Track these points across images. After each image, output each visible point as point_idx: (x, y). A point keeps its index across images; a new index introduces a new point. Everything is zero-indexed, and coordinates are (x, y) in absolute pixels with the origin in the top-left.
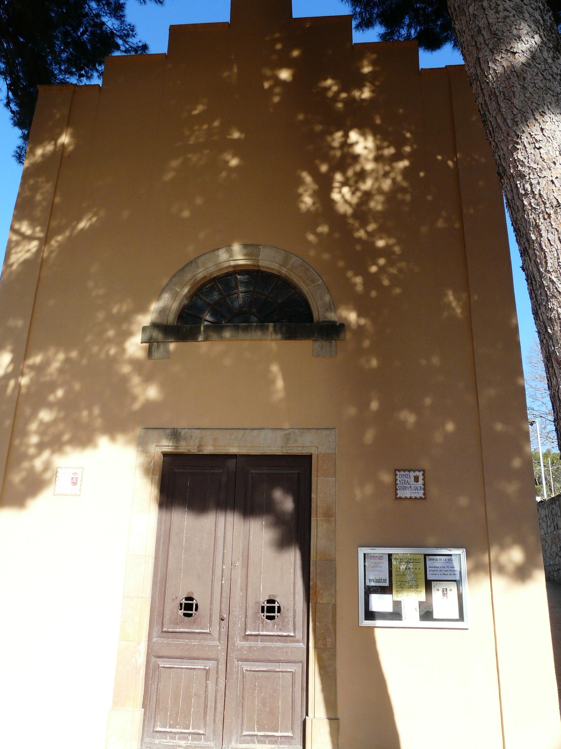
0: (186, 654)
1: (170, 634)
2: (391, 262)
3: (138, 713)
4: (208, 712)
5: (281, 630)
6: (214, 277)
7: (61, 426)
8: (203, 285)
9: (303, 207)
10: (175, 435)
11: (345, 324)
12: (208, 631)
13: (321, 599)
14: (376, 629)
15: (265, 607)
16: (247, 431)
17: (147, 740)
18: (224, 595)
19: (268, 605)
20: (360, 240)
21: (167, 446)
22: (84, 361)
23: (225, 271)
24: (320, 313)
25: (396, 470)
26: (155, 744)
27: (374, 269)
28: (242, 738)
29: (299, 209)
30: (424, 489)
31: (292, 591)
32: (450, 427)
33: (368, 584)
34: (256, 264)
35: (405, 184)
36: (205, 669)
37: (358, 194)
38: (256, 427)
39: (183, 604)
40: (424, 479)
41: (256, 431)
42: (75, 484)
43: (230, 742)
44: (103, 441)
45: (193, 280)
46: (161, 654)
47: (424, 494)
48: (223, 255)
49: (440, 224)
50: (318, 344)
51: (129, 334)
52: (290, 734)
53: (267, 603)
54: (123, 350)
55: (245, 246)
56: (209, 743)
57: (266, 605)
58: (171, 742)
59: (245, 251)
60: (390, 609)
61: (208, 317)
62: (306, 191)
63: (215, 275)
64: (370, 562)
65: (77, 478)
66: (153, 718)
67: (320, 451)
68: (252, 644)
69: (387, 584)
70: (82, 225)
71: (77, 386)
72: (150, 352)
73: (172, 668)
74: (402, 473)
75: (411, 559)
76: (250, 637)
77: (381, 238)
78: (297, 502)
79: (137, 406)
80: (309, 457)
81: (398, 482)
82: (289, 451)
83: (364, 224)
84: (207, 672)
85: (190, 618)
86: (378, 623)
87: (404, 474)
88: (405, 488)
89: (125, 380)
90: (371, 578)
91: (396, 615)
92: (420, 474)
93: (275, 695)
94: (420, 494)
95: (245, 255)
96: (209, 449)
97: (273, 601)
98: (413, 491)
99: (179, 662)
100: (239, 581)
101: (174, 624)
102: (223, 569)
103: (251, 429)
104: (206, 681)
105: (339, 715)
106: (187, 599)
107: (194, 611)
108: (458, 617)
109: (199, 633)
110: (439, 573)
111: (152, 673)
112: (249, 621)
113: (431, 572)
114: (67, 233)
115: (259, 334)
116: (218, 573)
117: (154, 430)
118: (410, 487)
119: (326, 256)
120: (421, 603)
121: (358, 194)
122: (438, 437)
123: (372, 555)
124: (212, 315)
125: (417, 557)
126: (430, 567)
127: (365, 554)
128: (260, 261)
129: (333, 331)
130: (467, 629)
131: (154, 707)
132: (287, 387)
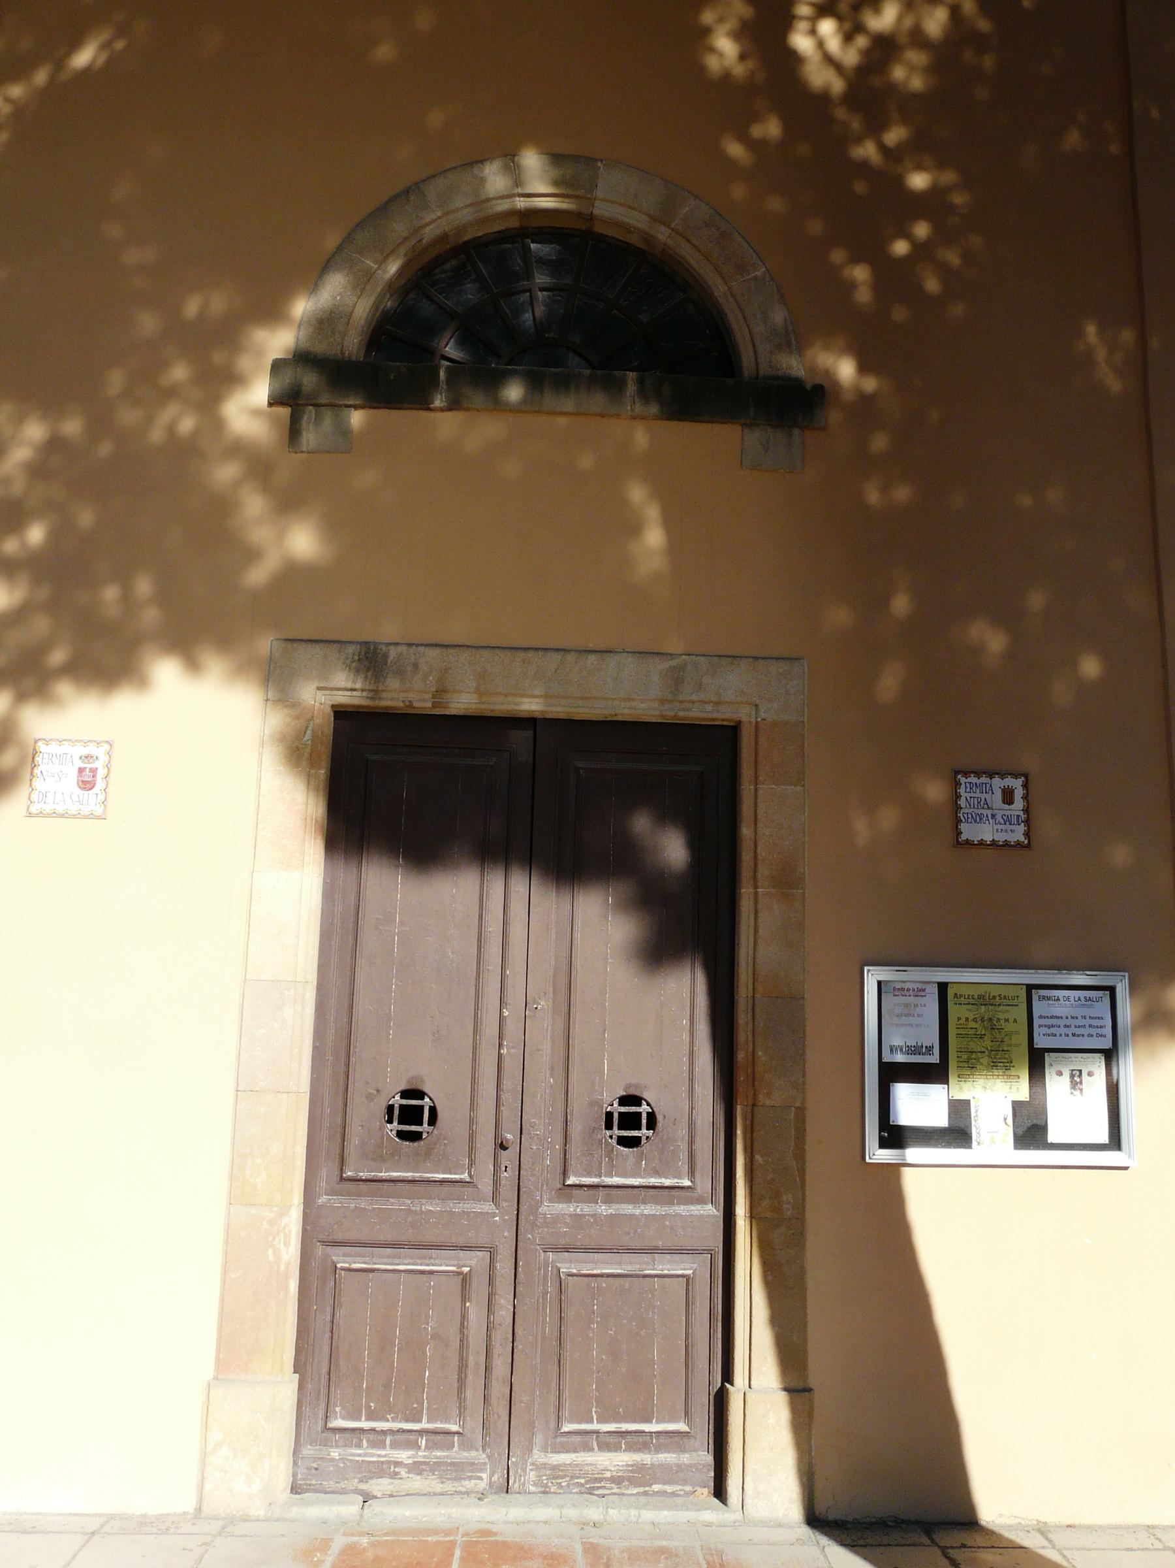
0: (408, 1235)
1: (363, 1187)
2: (944, 234)
3: (287, 1389)
4: (470, 1377)
5: (657, 1173)
6: (466, 243)
7: (41, 625)
8: (437, 261)
9: (713, 64)
10: (371, 660)
11: (826, 386)
12: (465, 1176)
13: (769, 1095)
14: (907, 1173)
15: (616, 1116)
16: (570, 658)
17: (308, 1450)
18: (507, 1083)
19: (623, 1109)
20: (863, 167)
21: (343, 687)
22: (105, 449)
23: (497, 227)
24: (759, 350)
25: (957, 773)
26: (333, 1460)
27: (901, 248)
28: (558, 1440)
29: (703, 69)
30: (1027, 822)
31: (686, 1075)
32: (1091, 667)
33: (887, 1058)
34: (585, 211)
35: (984, 25)
36: (460, 1273)
37: (861, 41)
38: (591, 646)
39: (396, 1106)
40: (1025, 797)
41: (592, 658)
42: (87, 785)
43: (529, 1450)
44: (166, 672)
45: (413, 242)
46: (339, 1237)
47: (1027, 834)
48: (495, 180)
49: (1073, 139)
50: (754, 437)
51: (230, 379)
52: (682, 1426)
53: (620, 1104)
54: (217, 424)
55: (556, 159)
56: (473, 1454)
57: (617, 1109)
58: (373, 1455)
59: (555, 173)
60: (940, 1119)
61: (451, 350)
62: (721, 20)
63: (468, 237)
64: (887, 1006)
65: (94, 771)
66: (323, 1398)
67: (763, 715)
68: (585, 1209)
69: (935, 1058)
70: (83, 58)
71: (86, 518)
72: (294, 432)
73: (373, 1270)
74: (973, 779)
75: (994, 997)
76: (575, 1192)
77: (919, 167)
78: (695, 845)
79: (258, 575)
80: (731, 733)
81: (962, 802)
82: (681, 714)
83: (875, 127)
84: (465, 1280)
85: (416, 1144)
86: (913, 1154)
87: (978, 781)
88: (978, 819)
89: (222, 507)
90: (896, 1044)
91: (957, 1133)
92: (1017, 784)
93: (643, 1333)
94: (1018, 834)
95: (556, 183)
96: (463, 702)
97: (635, 1100)
98: (999, 827)
99: (388, 1257)
100: (547, 1047)
101: (373, 1160)
102: (502, 1019)
103: (580, 651)
104: (464, 1301)
105: (812, 1382)
106: (405, 1094)
107: (425, 1125)
108: (1103, 1137)
109: (442, 1182)
110: (1063, 1030)
111: (318, 1284)
112: (575, 1149)
113: (1044, 1030)
114: (41, 77)
115: (598, 400)
116: (490, 1029)
117: (310, 645)
118: (993, 816)
119: (776, 204)
120: (1017, 1106)
121: (861, 41)
122: (1061, 694)
123: (898, 986)
124: (462, 344)
125: (1011, 992)
126: (1040, 1017)
127: (879, 983)
128: (597, 203)
129: (794, 404)
130: (1126, 1168)
131: (325, 1370)
132: (674, 546)
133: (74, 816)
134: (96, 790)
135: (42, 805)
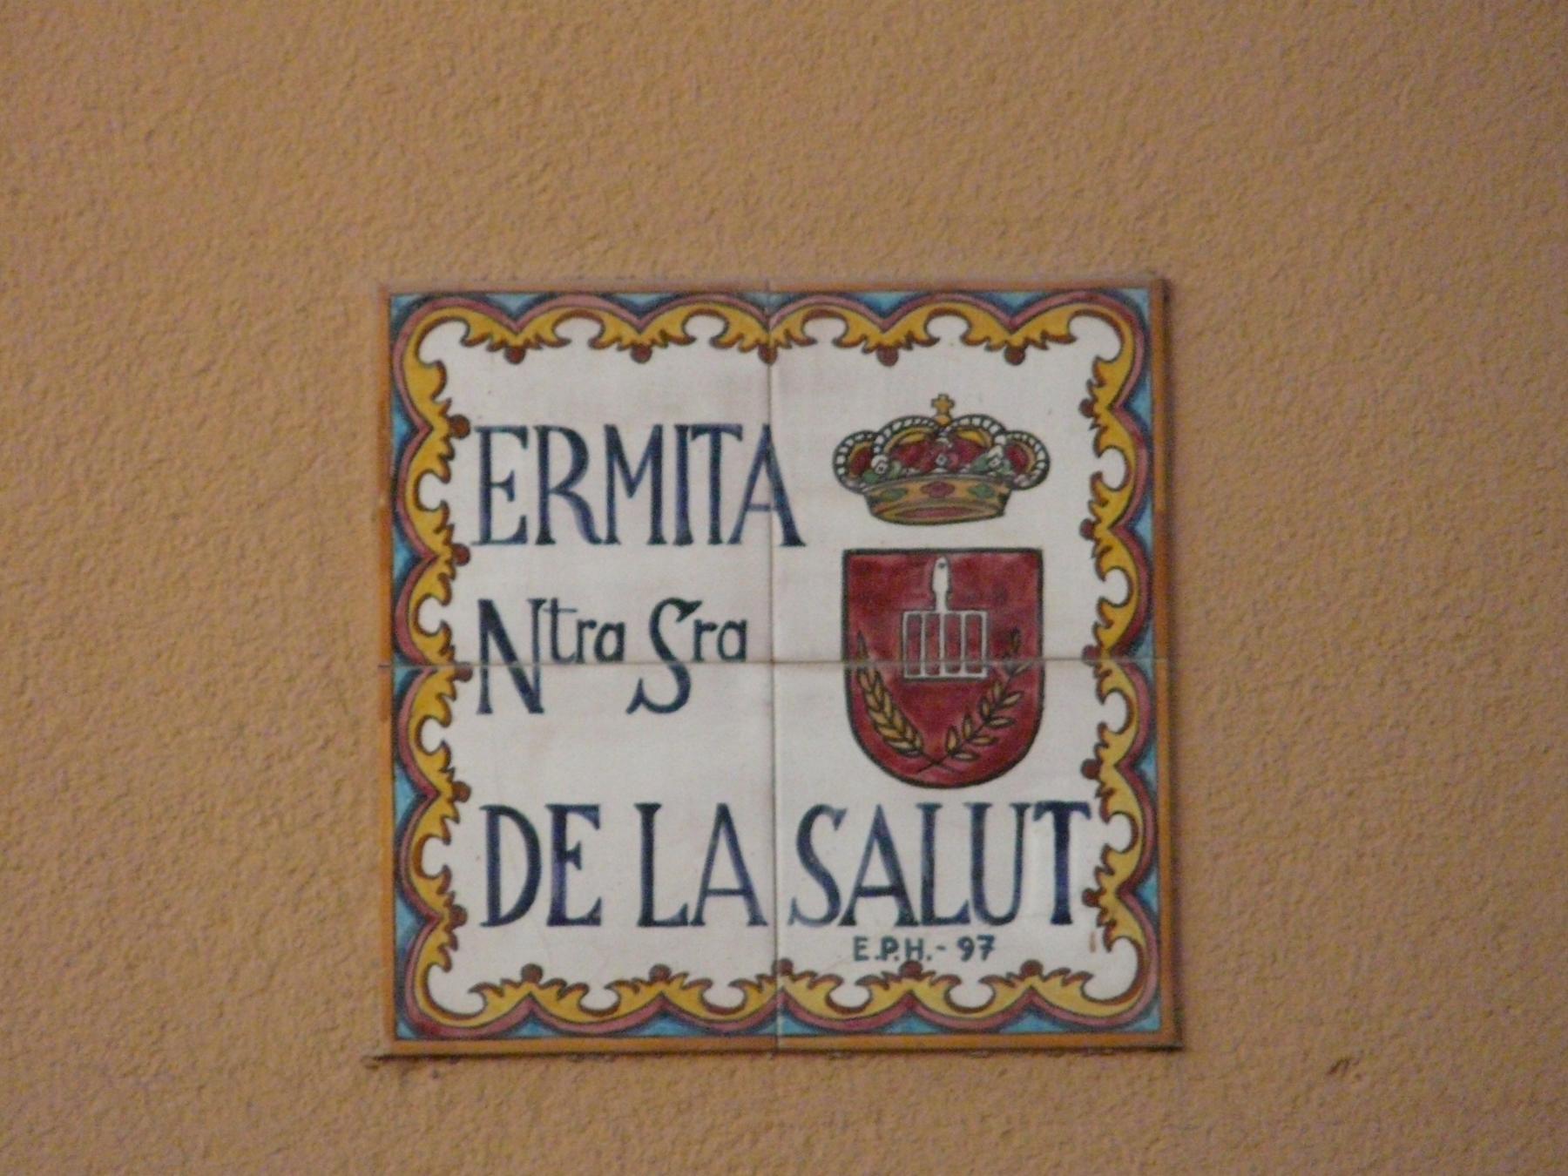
65: (1012, 581)
133: (853, 1036)
134: (1053, 765)
135: (531, 940)
